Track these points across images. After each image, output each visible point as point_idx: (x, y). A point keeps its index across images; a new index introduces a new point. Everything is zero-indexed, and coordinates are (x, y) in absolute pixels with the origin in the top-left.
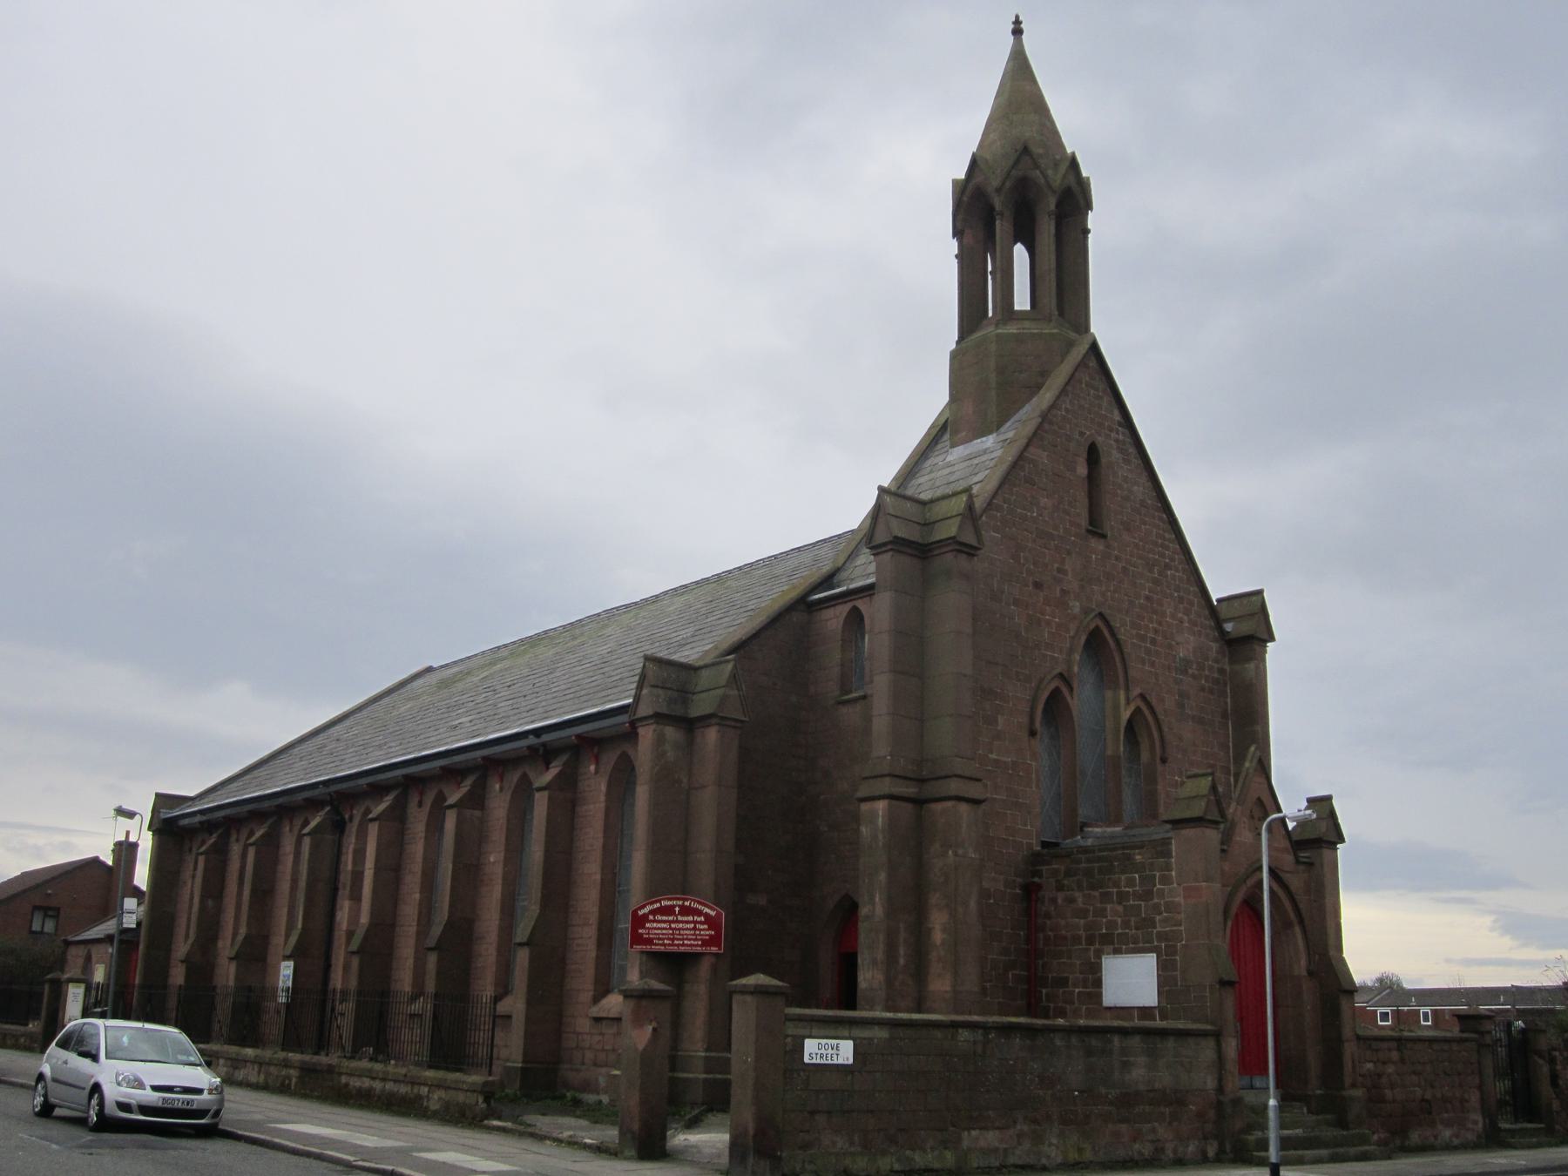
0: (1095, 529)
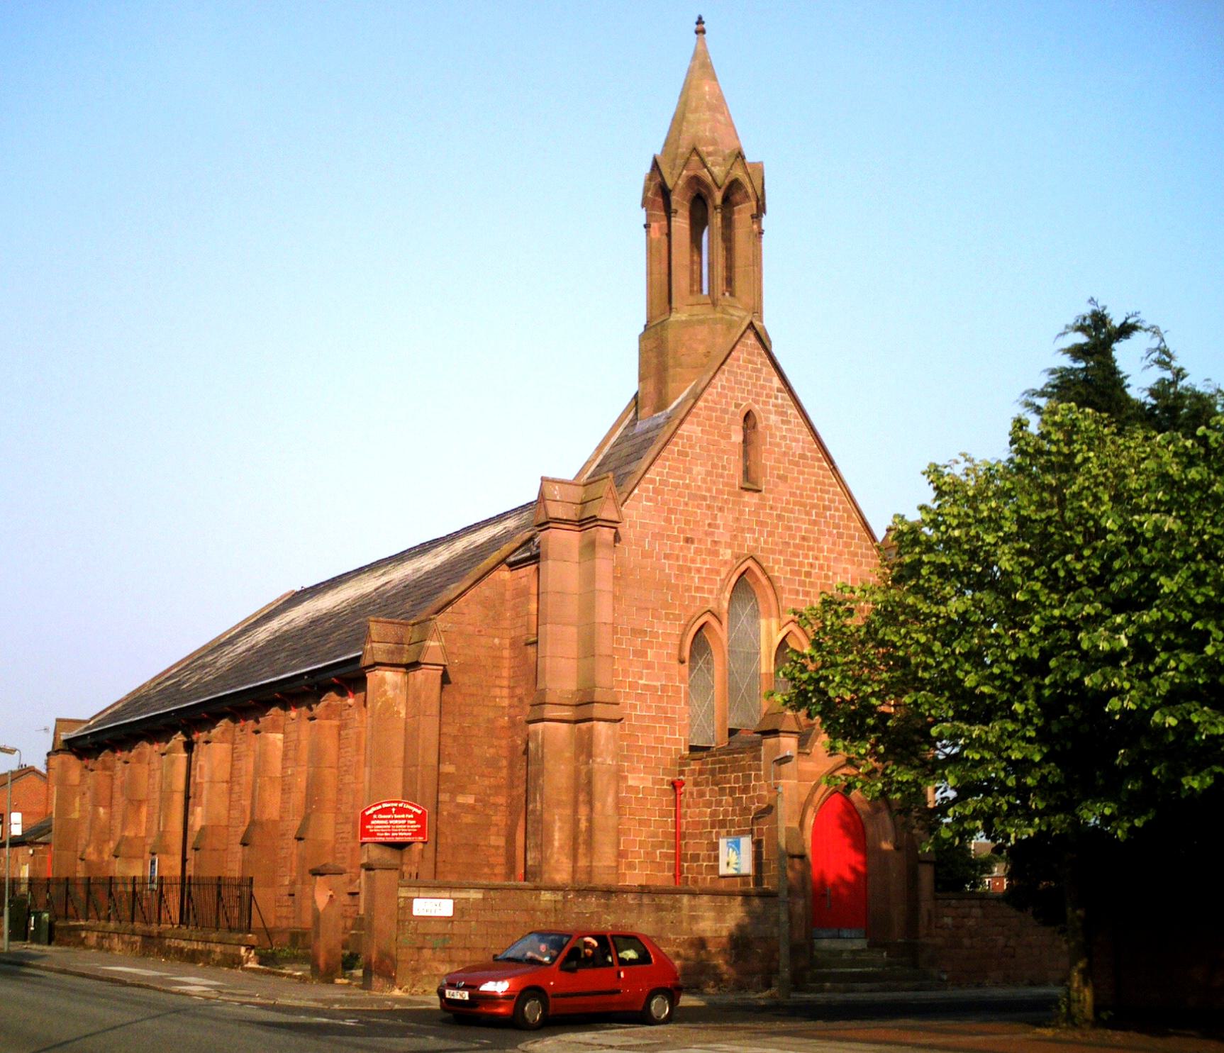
0: (750, 483)
